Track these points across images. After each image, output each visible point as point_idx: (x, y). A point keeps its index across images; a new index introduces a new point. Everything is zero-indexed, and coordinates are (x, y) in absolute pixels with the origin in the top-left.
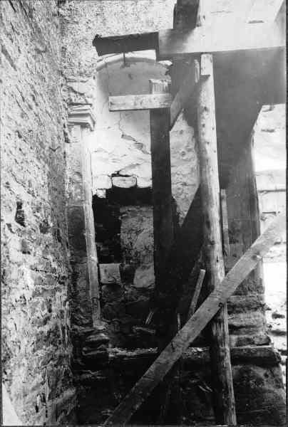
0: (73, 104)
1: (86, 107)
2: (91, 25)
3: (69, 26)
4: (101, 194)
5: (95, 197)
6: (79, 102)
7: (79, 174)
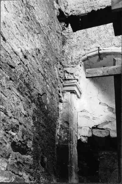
0: (65, 80)
1: (74, 81)
2: (79, 39)
3: (67, 40)
4: (84, 140)
5: (79, 141)
6: (70, 78)
7: (67, 123)
